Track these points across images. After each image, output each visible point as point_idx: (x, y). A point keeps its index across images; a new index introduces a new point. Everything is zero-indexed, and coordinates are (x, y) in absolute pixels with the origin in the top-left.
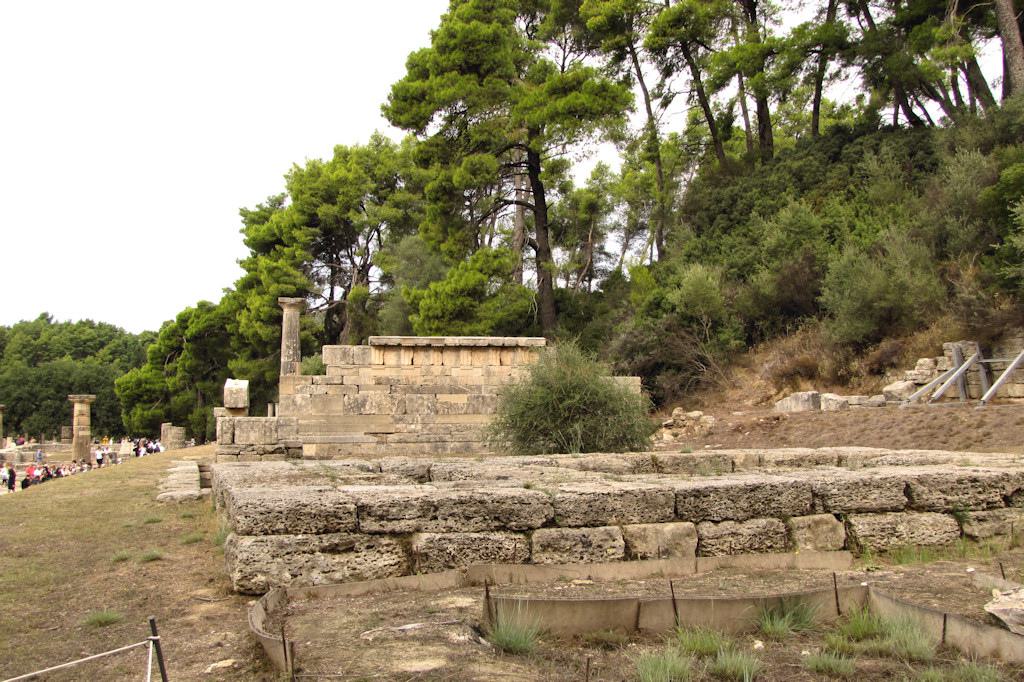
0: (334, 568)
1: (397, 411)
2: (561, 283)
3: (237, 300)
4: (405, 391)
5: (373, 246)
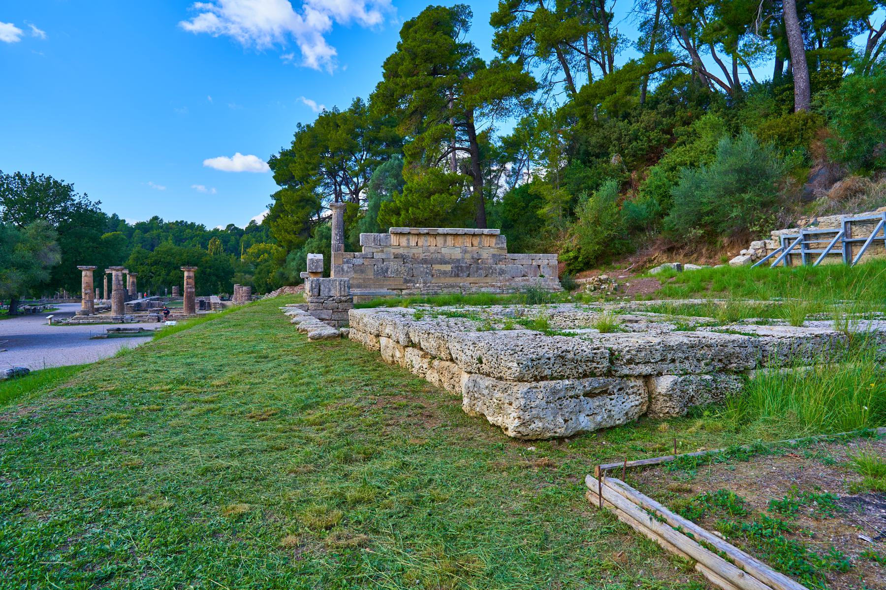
0: (595, 411)
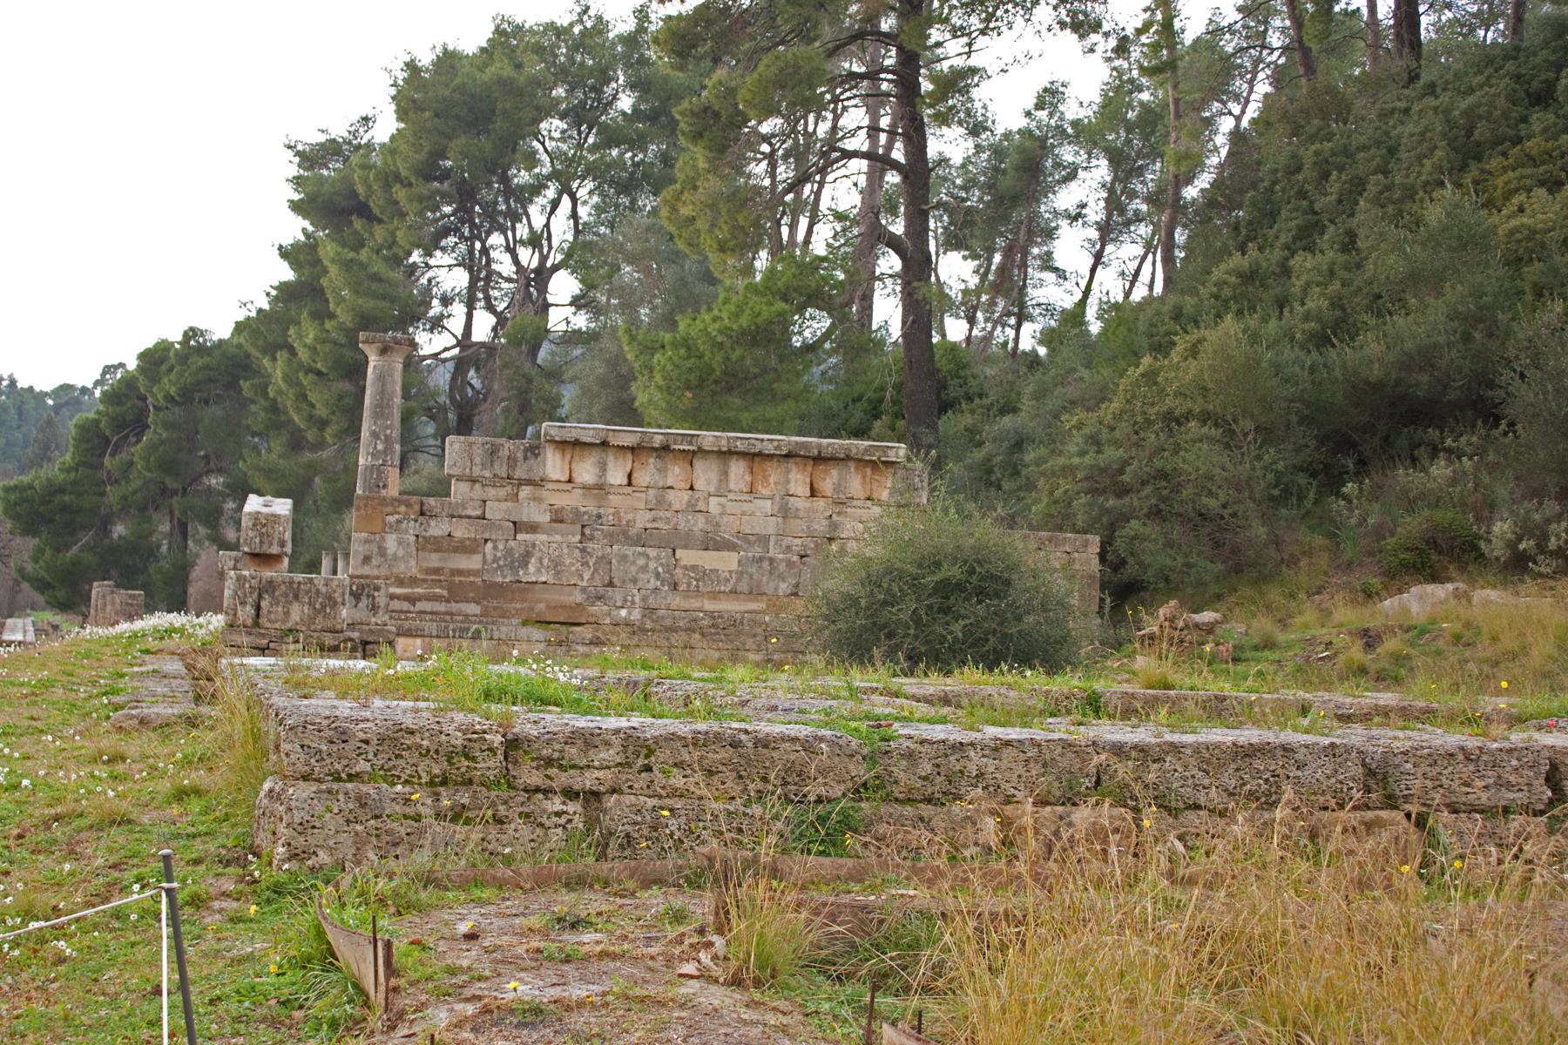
1: (592, 577)
2: (955, 329)
3: (263, 330)
4: (612, 539)
5: (562, 229)
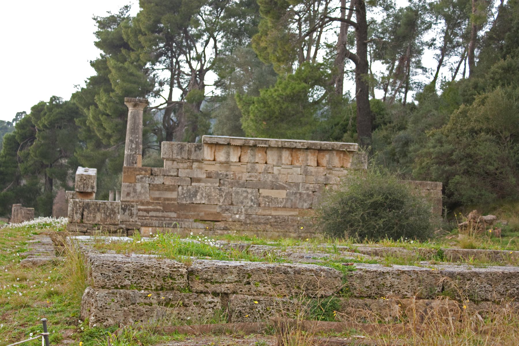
1: (224, 202)
2: (379, 94)
3: (84, 97)
4: (232, 185)
